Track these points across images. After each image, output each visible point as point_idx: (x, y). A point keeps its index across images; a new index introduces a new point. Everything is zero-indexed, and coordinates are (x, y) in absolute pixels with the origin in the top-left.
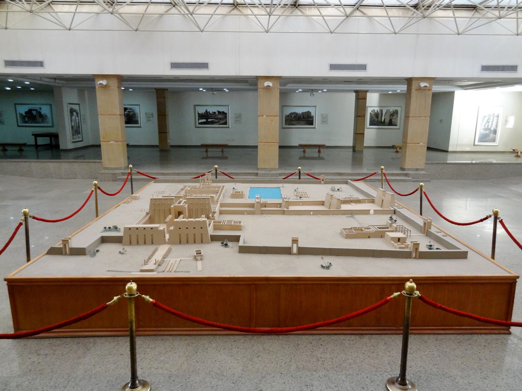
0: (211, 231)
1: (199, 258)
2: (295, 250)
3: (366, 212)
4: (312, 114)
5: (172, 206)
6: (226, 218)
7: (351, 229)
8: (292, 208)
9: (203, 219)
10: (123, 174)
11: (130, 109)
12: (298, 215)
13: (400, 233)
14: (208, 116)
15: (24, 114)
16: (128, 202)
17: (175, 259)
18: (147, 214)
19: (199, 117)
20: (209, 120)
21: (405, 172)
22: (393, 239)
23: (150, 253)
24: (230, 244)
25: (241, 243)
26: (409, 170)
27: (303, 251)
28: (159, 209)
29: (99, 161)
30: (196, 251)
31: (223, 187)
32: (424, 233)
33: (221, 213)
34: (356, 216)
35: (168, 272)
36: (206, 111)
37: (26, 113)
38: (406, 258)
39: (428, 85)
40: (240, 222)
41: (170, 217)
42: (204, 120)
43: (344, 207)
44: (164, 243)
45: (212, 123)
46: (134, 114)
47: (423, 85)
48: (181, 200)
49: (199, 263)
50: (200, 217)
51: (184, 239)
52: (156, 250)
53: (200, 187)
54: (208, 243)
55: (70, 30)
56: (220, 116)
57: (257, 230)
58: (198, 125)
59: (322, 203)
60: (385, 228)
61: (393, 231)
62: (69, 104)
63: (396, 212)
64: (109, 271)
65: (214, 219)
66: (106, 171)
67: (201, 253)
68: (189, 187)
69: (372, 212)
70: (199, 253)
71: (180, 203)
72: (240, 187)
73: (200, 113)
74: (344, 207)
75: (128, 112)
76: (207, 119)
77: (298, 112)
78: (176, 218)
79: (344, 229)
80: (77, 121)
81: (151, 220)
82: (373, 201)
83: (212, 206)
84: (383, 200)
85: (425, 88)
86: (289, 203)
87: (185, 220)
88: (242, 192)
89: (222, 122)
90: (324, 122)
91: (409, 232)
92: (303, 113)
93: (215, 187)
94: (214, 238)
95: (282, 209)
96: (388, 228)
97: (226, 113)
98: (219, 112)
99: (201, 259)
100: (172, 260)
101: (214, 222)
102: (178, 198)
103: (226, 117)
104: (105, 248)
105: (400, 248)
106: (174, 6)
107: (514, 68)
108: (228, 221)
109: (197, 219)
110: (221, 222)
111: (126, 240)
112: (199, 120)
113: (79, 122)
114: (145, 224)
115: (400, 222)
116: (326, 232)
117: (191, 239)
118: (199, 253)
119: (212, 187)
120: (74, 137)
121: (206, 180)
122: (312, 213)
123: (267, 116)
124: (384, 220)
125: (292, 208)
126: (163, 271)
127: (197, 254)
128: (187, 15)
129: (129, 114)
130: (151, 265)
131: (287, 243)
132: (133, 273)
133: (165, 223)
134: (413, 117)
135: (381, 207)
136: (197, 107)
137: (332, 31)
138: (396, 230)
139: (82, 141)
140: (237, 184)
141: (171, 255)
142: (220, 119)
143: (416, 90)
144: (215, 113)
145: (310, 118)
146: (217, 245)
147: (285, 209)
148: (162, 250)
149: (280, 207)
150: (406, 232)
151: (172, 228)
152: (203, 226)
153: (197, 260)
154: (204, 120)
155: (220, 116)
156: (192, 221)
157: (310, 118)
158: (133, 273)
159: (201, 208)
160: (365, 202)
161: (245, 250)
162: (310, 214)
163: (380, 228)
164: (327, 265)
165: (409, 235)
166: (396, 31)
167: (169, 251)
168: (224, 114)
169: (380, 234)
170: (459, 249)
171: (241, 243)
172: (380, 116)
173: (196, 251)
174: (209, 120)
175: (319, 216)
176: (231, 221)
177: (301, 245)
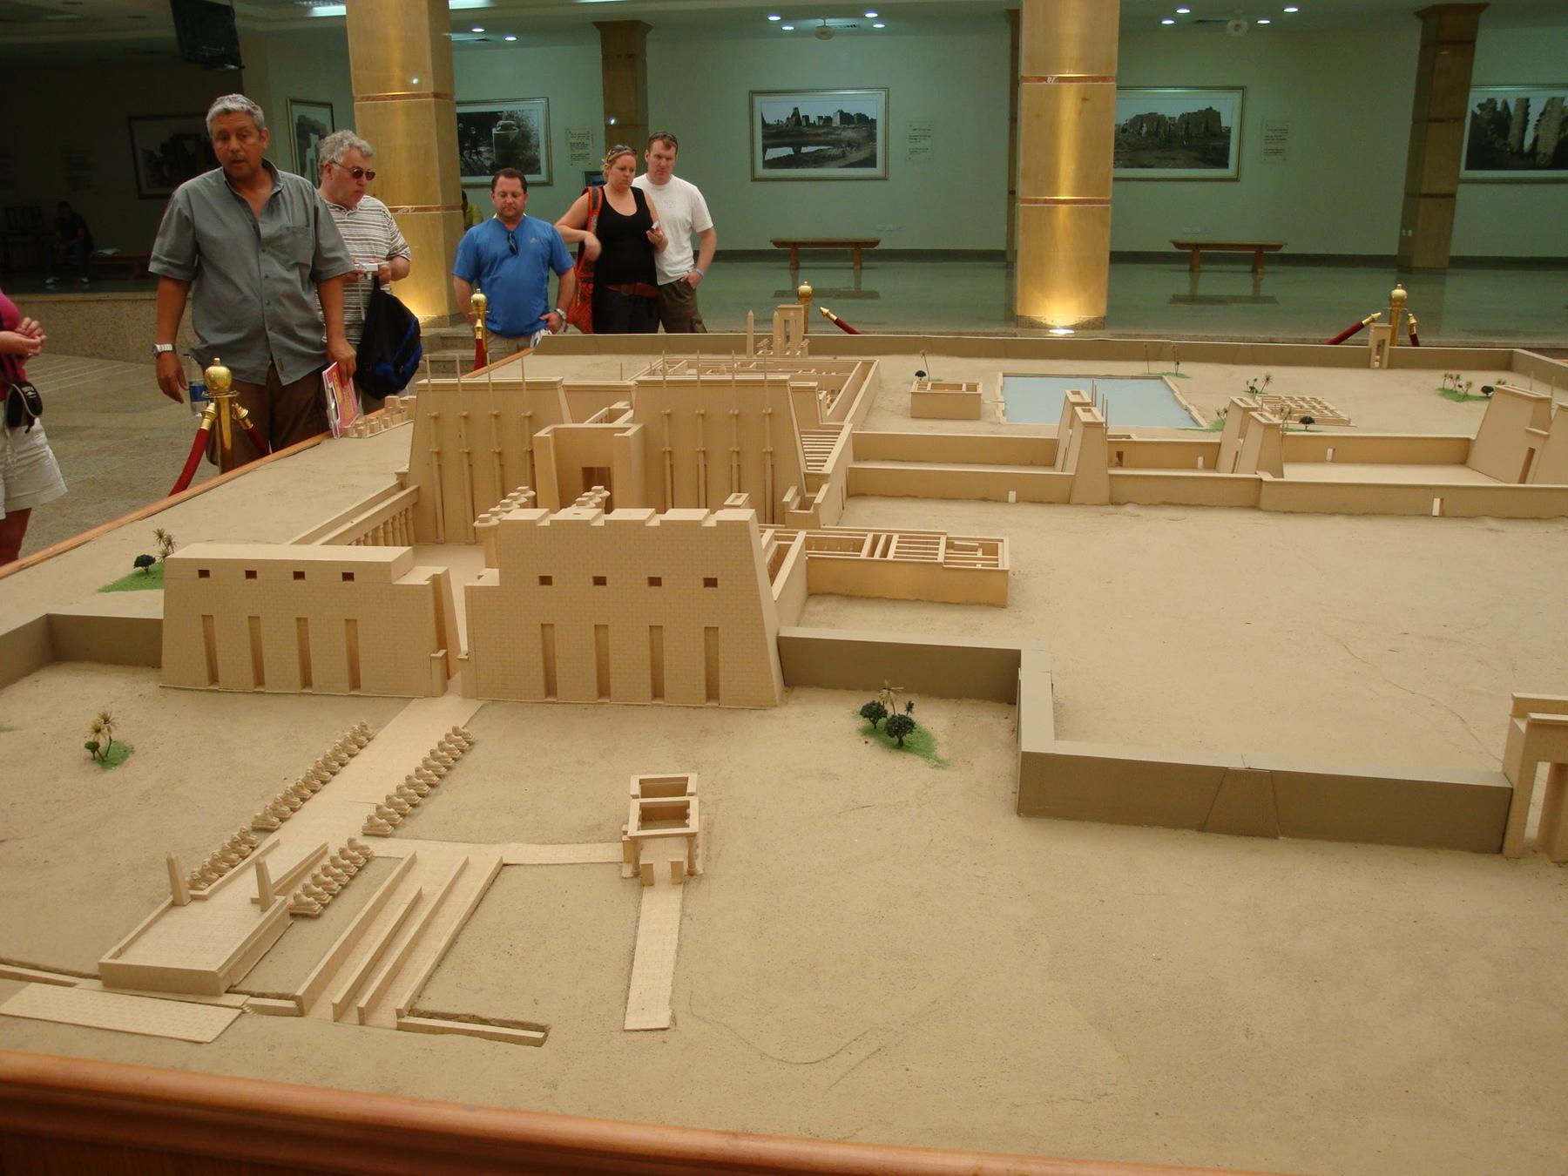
1: (663, 853)
4: (1225, 123)
6: (892, 523)
9: (737, 510)
11: (511, 116)
12: (1350, 514)
14: (803, 134)
15: (158, 153)
17: (460, 852)
19: (765, 137)
20: (804, 150)
24: (931, 718)
30: (648, 788)
33: (858, 489)
35: (340, 1011)
36: (796, 112)
37: (164, 147)
40: (991, 549)
42: (788, 151)
45: (818, 160)
46: (525, 136)
48: (619, 405)
49: (661, 910)
51: (576, 668)
52: (359, 741)
54: (762, 705)
56: (849, 134)
58: (761, 171)
62: (293, 101)
65: (813, 522)
67: (679, 814)
70: (664, 808)
71: (612, 417)
73: (770, 121)
75: (504, 127)
76: (797, 147)
77: (1168, 115)
83: (806, 445)
88: (972, 387)
89: (855, 156)
90: (1278, 152)
92: (1187, 118)
94: (806, 669)
97: (874, 121)
98: (846, 118)
99: (686, 876)
101: (808, 543)
103: (871, 137)
111: (180, 649)
114: (372, 537)
117: (630, 667)
118: (664, 808)
121: (779, 340)
127: (649, 817)
129: (506, 137)
136: (758, 100)
140: (930, 359)
142: (849, 144)
144: (829, 120)
145: (1215, 136)
146: (829, 727)
147: (1267, 477)
148: (404, 742)
152: (720, 572)
154: (788, 151)
155: (849, 134)
157: (1215, 136)
158: (32, 1000)
161: (1065, 793)
162: (1428, 515)
170: (327, 543)
171: (1038, 737)
172: (1514, 130)
173: (648, 788)
174: (804, 150)
176: (931, 540)
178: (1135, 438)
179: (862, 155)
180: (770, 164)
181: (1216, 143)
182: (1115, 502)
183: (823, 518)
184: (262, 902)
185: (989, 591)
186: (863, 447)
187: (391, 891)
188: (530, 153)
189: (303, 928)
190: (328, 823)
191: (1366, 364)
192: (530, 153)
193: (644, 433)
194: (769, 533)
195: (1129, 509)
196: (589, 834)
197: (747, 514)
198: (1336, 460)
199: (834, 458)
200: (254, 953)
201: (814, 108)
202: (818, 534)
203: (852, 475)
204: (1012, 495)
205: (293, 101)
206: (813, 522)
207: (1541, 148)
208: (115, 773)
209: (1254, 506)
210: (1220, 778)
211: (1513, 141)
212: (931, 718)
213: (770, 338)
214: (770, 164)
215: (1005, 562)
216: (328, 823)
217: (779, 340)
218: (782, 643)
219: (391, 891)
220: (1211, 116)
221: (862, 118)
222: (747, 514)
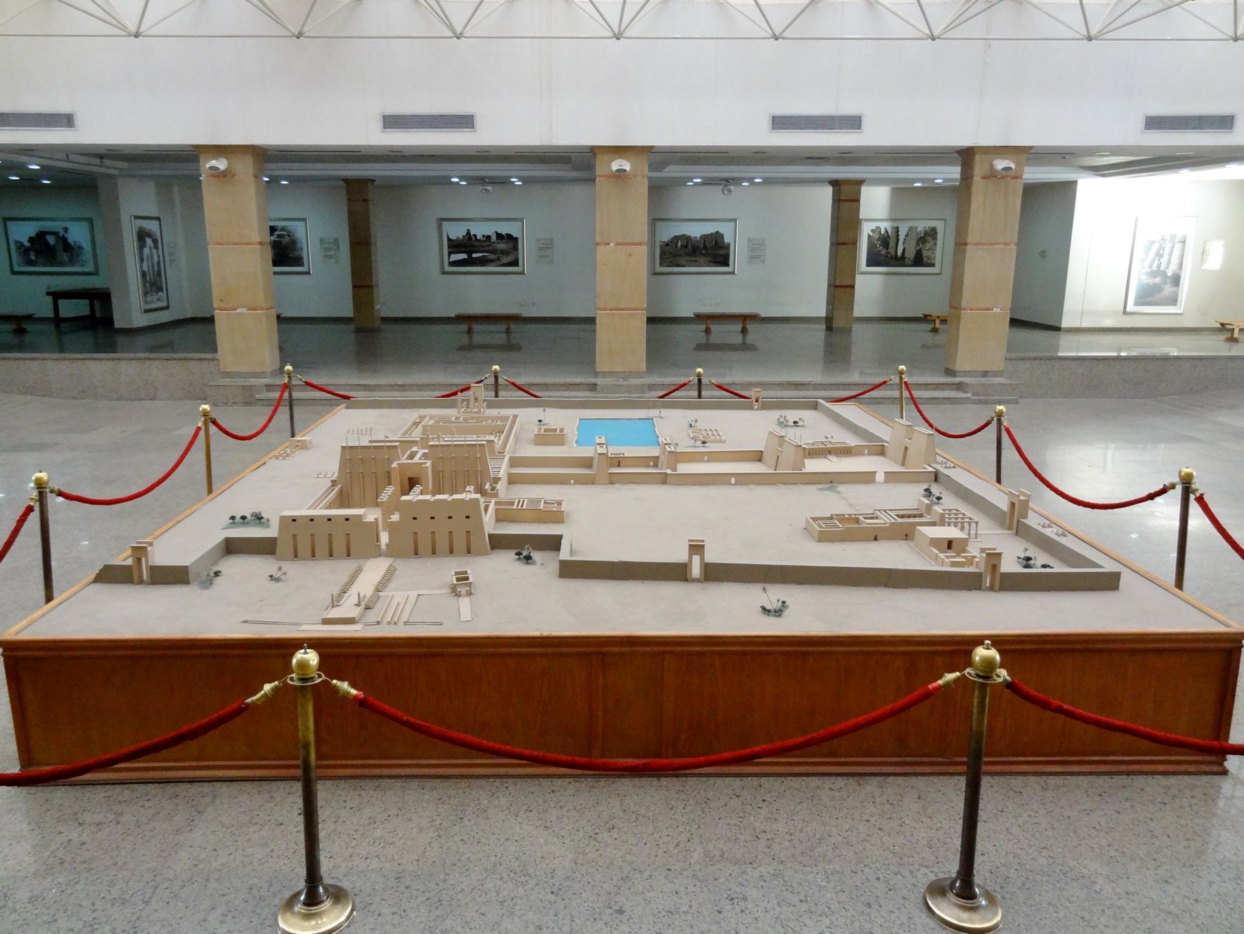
0: (489, 524)
1: (463, 590)
2: (696, 571)
3: (866, 478)
5: (394, 465)
7: (831, 518)
8: (684, 468)
9: (470, 495)
10: (269, 387)
11: (283, 229)
13: (952, 528)
14: (473, 246)
15: (27, 244)
16: (286, 456)
17: (406, 594)
18: (334, 483)
22: (935, 542)
23: (344, 579)
24: (536, 555)
25: (564, 554)
26: (966, 373)
27: (717, 574)
28: (362, 472)
30: (456, 573)
31: (515, 417)
32: (1010, 528)
33: (513, 480)
34: (841, 488)
36: (468, 233)
37: (31, 240)
38: (969, 589)
39: (1013, 166)
40: (559, 503)
41: (390, 490)
42: (464, 256)
43: (814, 465)
45: (482, 262)
46: (293, 242)
49: (465, 602)
51: (425, 544)
52: (358, 571)
54: (485, 554)
55: (137, 36)
57: (600, 522)
58: (448, 268)
59: (758, 457)
61: (933, 524)
63: (940, 477)
64: (246, 622)
65: (496, 495)
66: (227, 381)
67: (467, 579)
69: (880, 477)
70: (463, 578)
71: (412, 456)
72: (556, 418)
73: (453, 237)
74: (814, 465)
75: (279, 236)
79: (815, 519)
80: (156, 259)
81: (343, 500)
82: (881, 451)
83: (491, 464)
84: (906, 448)
85: (1004, 173)
86: (677, 457)
88: (562, 430)
89: (505, 260)
91: (973, 525)
92: (704, 237)
94: (498, 543)
95: (660, 471)
96: (921, 516)
97: (516, 239)
98: (499, 236)
99: (469, 594)
103: (516, 248)
105: (954, 564)
107: (1225, 122)
108: (531, 501)
109: (456, 496)
110: (513, 503)
111: (284, 547)
112: (450, 254)
113: (159, 263)
114: (329, 507)
115: (949, 502)
116: (769, 525)
117: (442, 543)
118: (463, 578)
120: (149, 299)
122: (733, 480)
123: (618, 244)
124: (910, 496)
125: (684, 468)
127: (458, 580)
129: (280, 243)
130: (347, 608)
131: (677, 554)
133: (377, 505)
134: (976, 244)
135: (903, 464)
136: (444, 223)
138: (942, 522)
139: (167, 308)
141: (392, 585)
142: (502, 252)
143: (984, 178)
144: (489, 237)
146: (505, 560)
147: (669, 471)
148: (374, 571)
149: (656, 466)
150: (966, 525)
151: (395, 517)
152: (471, 513)
153: (458, 595)
154: (464, 256)
159: (463, 467)
160: (862, 454)
161: (573, 570)
163: (902, 516)
165: (973, 532)
169: (903, 531)
171: (564, 554)
172: (892, 244)
173: (456, 573)
175: (752, 487)
176: (538, 501)
177: (710, 557)
179: (510, 258)
180: (453, 264)
181: (722, 252)
182: (612, 483)
185: (557, 517)
188: (297, 253)
191: (751, 408)
192: (297, 253)
195: (617, 486)
196: (440, 588)
199: (503, 470)
201: (480, 230)
203: (510, 475)
205: (137, 217)
207: (907, 255)
209: (664, 483)
210: (612, 564)
211: (892, 251)
212: (536, 555)
214: (453, 264)
218: (490, 536)
220: (717, 237)
221: (509, 237)
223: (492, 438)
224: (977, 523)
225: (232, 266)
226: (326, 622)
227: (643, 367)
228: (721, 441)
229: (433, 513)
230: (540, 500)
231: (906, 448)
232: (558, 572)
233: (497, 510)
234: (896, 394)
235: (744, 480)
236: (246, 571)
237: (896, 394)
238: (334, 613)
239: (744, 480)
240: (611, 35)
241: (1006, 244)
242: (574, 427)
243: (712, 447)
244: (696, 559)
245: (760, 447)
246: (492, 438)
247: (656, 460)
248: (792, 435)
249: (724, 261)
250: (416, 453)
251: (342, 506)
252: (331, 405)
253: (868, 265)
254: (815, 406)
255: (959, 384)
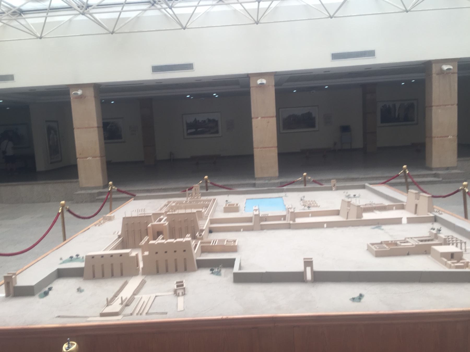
0: (197, 255)
1: (180, 292)
2: (309, 276)
3: (398, 221)
5: (149, 225)
6: (216, 237)
7: (381, 243)
8: (299, 220)
9: (188, 238)
10: (101, 194)
16: (100, 224)
18: (119, 237)
21: (434, 172)
22: (444, 255)
23: (118, 289)
25: (236, 269)
26: (437, 169)
27: (322, 277)
28: (134, 231)
29: (75, 180)
30: (177, 283)
31: (214, 200)
34: (384, 227)
35: (137, 314)
36: (195, 119)
39: (451, 67)
40: (235, 241)
41: (146, 239)
42: (193, 130)
43: (367, 216)
44: (135, 273)
45: (202, 132)
47: (445, 67)
48: (162, 217)
49: (181, 299)
50: (184, 237)
52: (126, 283)
53: (186, 202)
55: (41, 38)
57: (259, 251)
59: (337, 213)
60: (429, 240)
61: (441, 244)
64: (59, 317)
65: (202, 239)
66: (83, 192)
67: (183, 285)
68: (174, 202)
69: (404, 221)
70: (180, 285)
71: (160, 220)
72: (234, 199)
74: (367, 216)
78: (155, 239)
79: (373, 244)
81: (123, 244)
82: (402, 207)
84: (416, 205)
85: (448, 71)
86: (294, 215)
87: (163, 241)
88: (237, 205)
91: (463, 244)
93: (204, 201)
94: (202, 264)
95: (289, 223)
96: (432, 240)
98: (209, 121)
99: (184, 294)
100: (145, 296)
101: (201, 243)
102: (156, 215)
104: (60, 286)
105: (457, 267)
106: (153, 5)
108: (220, 241)
109: (178, 240)
110: (210, 243)
112: (187, 130)
114: (116, 248)
115: (445, 233)
116: (349, 249)
118: (180, 285)
119: (201, 201)
121: (194, 194)
122: (325, 225)
123: (262, 118)
124: (424, 230)
125: (299, 220)
126: (131, 314)
127: (178, 286)
128: (165, 9)
130: (116, 307)
131: (298, 267)
132: (90, 319)
133: (140, 247)
134: (437, 106)
137: (332, 15)
138: (446, 242)
141: (143, 291)
143: (438, 74)
144: (204, 121)
146: (205, 274)
147: (291, 222)
149: (285, 219)
150: (459, 245)
151: (146, 253)
152: (186, 248)
153: (178, 295)
154: (193, 130)
156: (172, 243)
158: (90, 319)
159: (184, 225)
160: (392, 209)
161: (242, 278)
163: (422, 241)
164: (357, 295)
165: (463, 248)
166: (408, 9)
167: (142, 284)
168: (215, 122)
171: (236, 269)
173: (177, 283)
175: (335, 228)
176: (224, 241)
177: (317, 268)
178: (269, 215)
183: (204, 238)
184: (122, 304)
185: (234, 249)
186: (212, 221)
187: (139, 302)
189: (127, 307)
190: (127, 293)
193: (169, 224)
194: (194, 241)
195: (265, 231)
196: (168, 291)
197: (190, 239)
198: (312, 216)
200: (122, 310)
201: (201, 118)
202: (203, 241)
204: (242, 230)
206: (202, 239)
208: (83, 293)
213: (192, 193)
215: (236, 244)
216: (127, 293)
217: (194, 194)
219: (139, 302)
220: (309, 114)
222: (190, 239)
223: (201, 210)
224: (465, 243)
225: (87, 137)
226: (102, 315)
227: (277, 174)
228: (317, 206)
229: (165, 248)
230: (224, 240)
231: (416, 205)
232: (232, 279)
233: (202, 247)
234: (403, 180)
235: (331, 225)
236: (63, 287)
237: (403, 180)
238: (108, 310)
239: (331, 225)
240: (254, 22)
241: (452, 105)
242: (247, 204)
243: (313, 209)
244: (309, 269)
245: (338, 208)
246: (201, 210)
247: (284, 217)
248: (355, 201)
249: (313, 126)
250: (162, 219)
251: (123, 248)
252: (127, 199)
253: (381, 123)
254: (364, 187)
255: (435, 174)
